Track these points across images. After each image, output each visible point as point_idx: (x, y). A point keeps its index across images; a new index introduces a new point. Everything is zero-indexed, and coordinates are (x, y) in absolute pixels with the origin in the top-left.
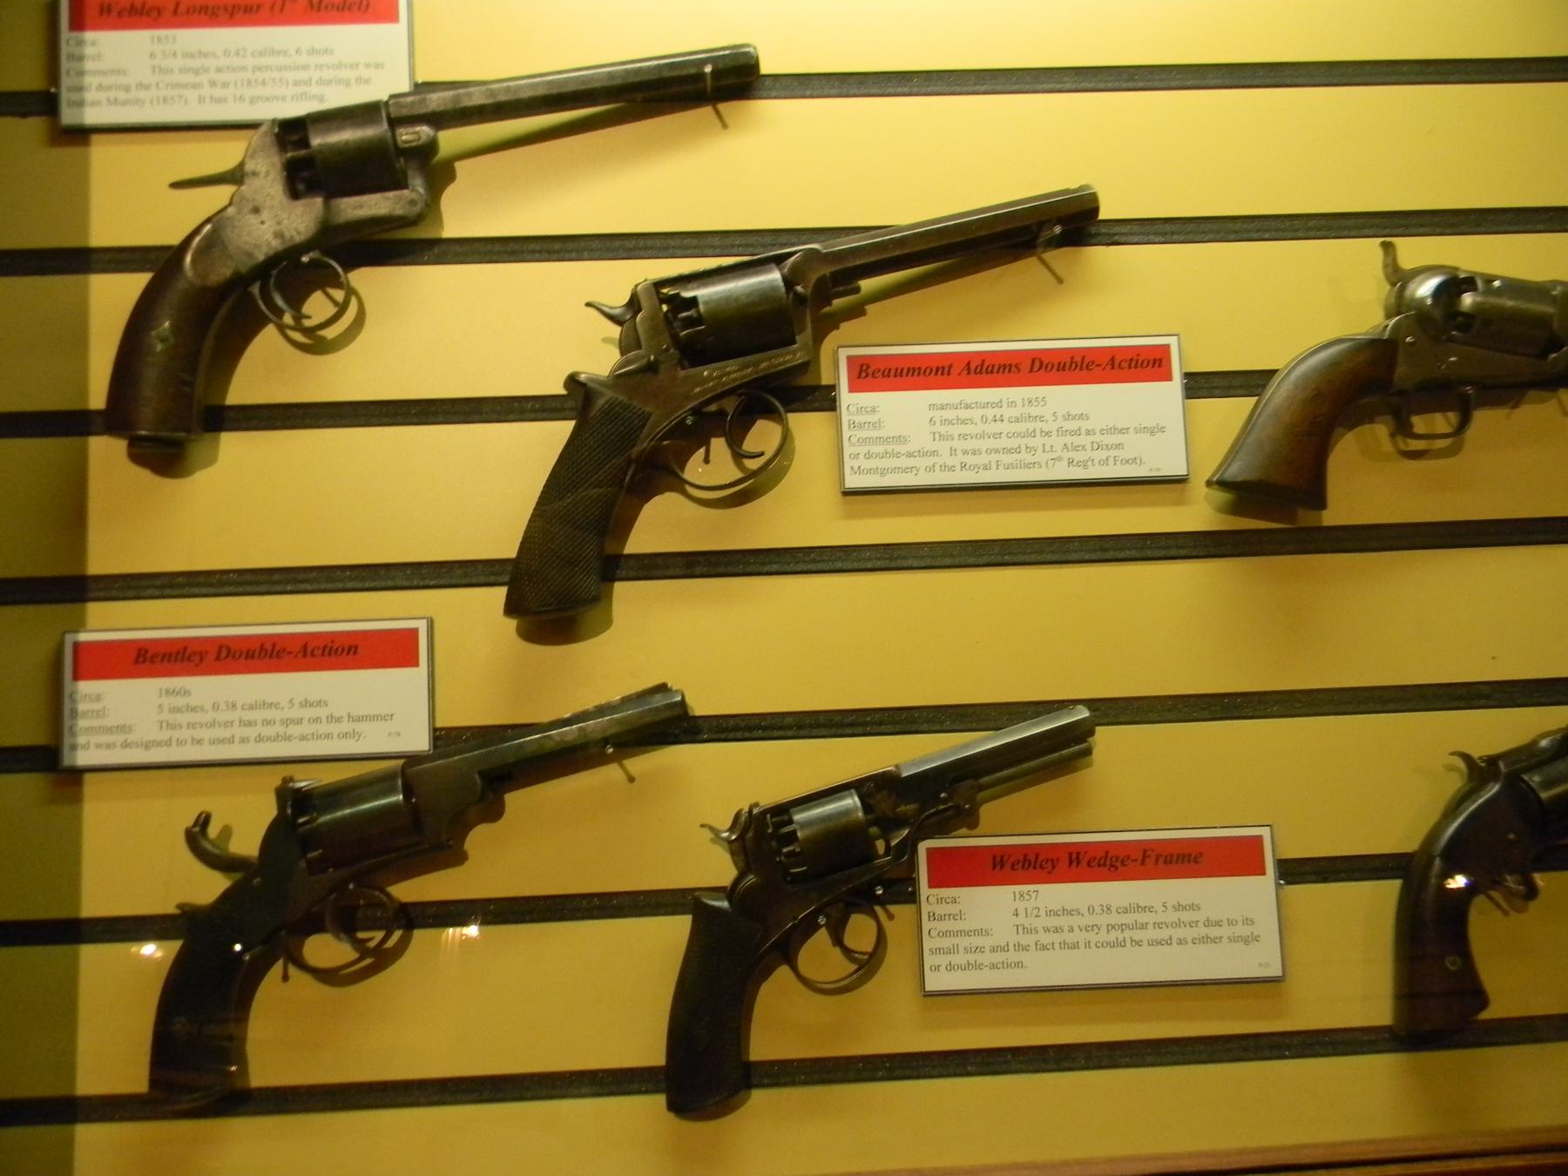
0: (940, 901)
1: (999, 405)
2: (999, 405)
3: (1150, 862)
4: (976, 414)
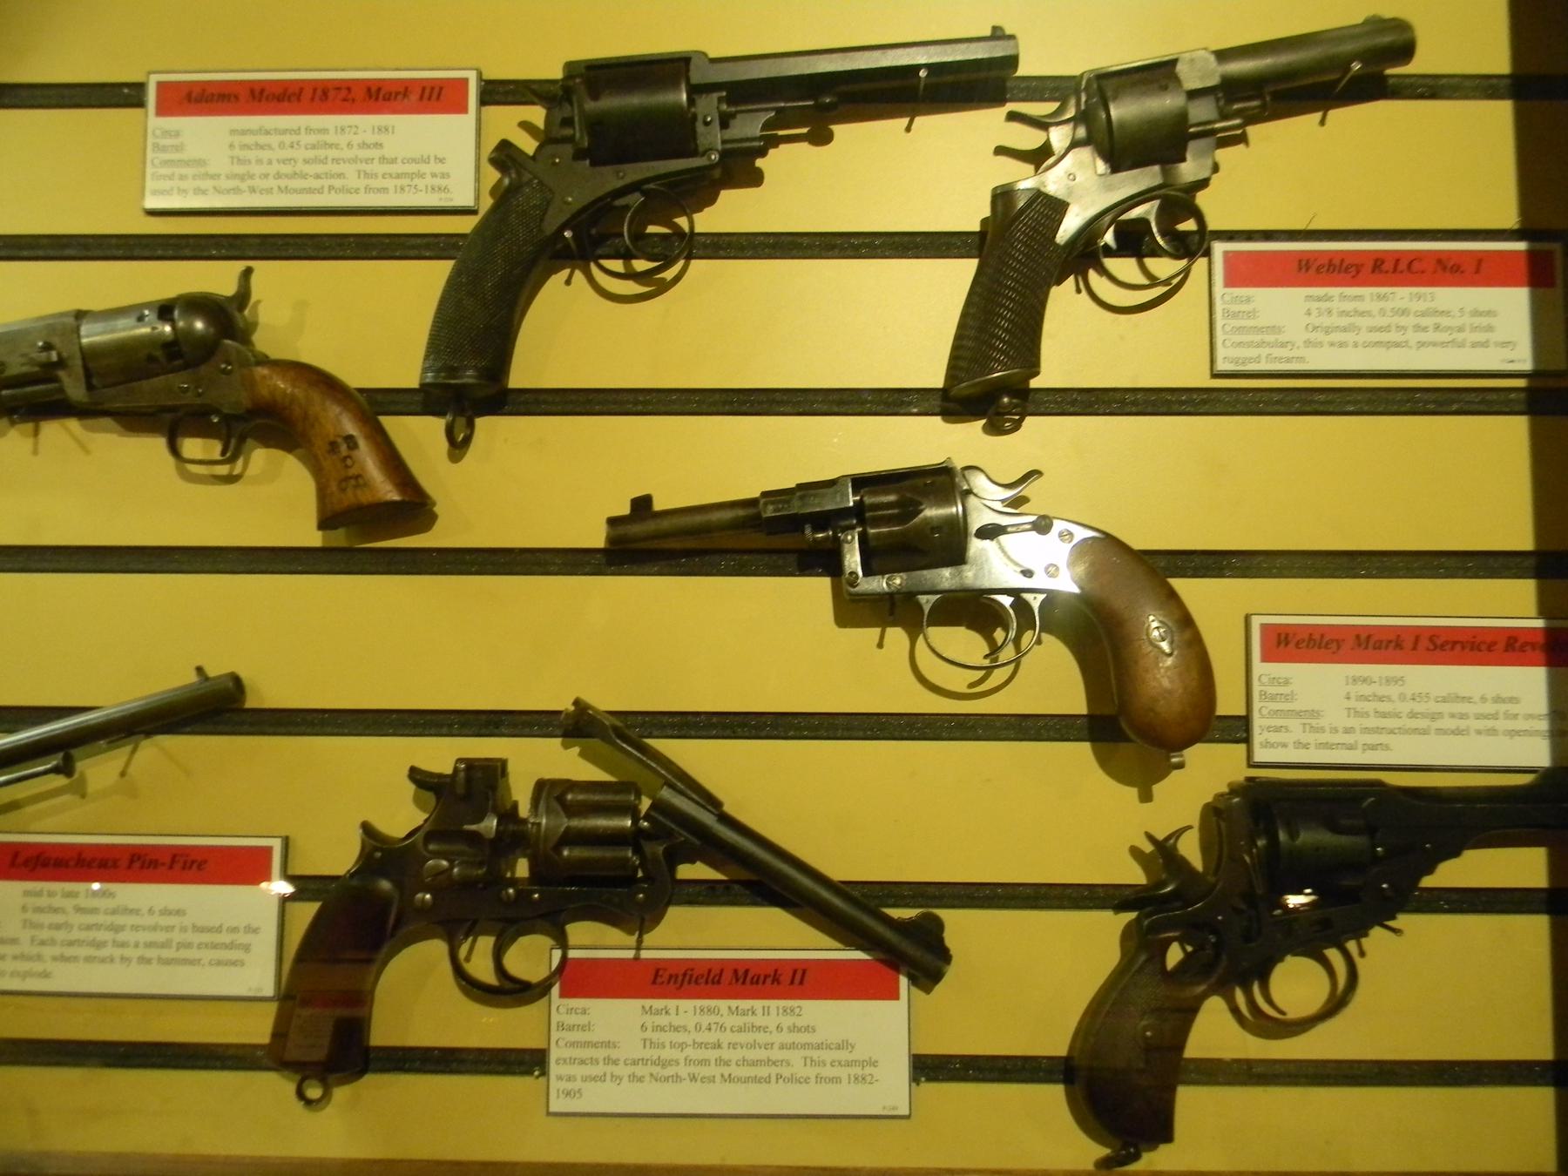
0: (570, 1011)
1: (297, 131)
2: (297, 131)
4: (274, 140)
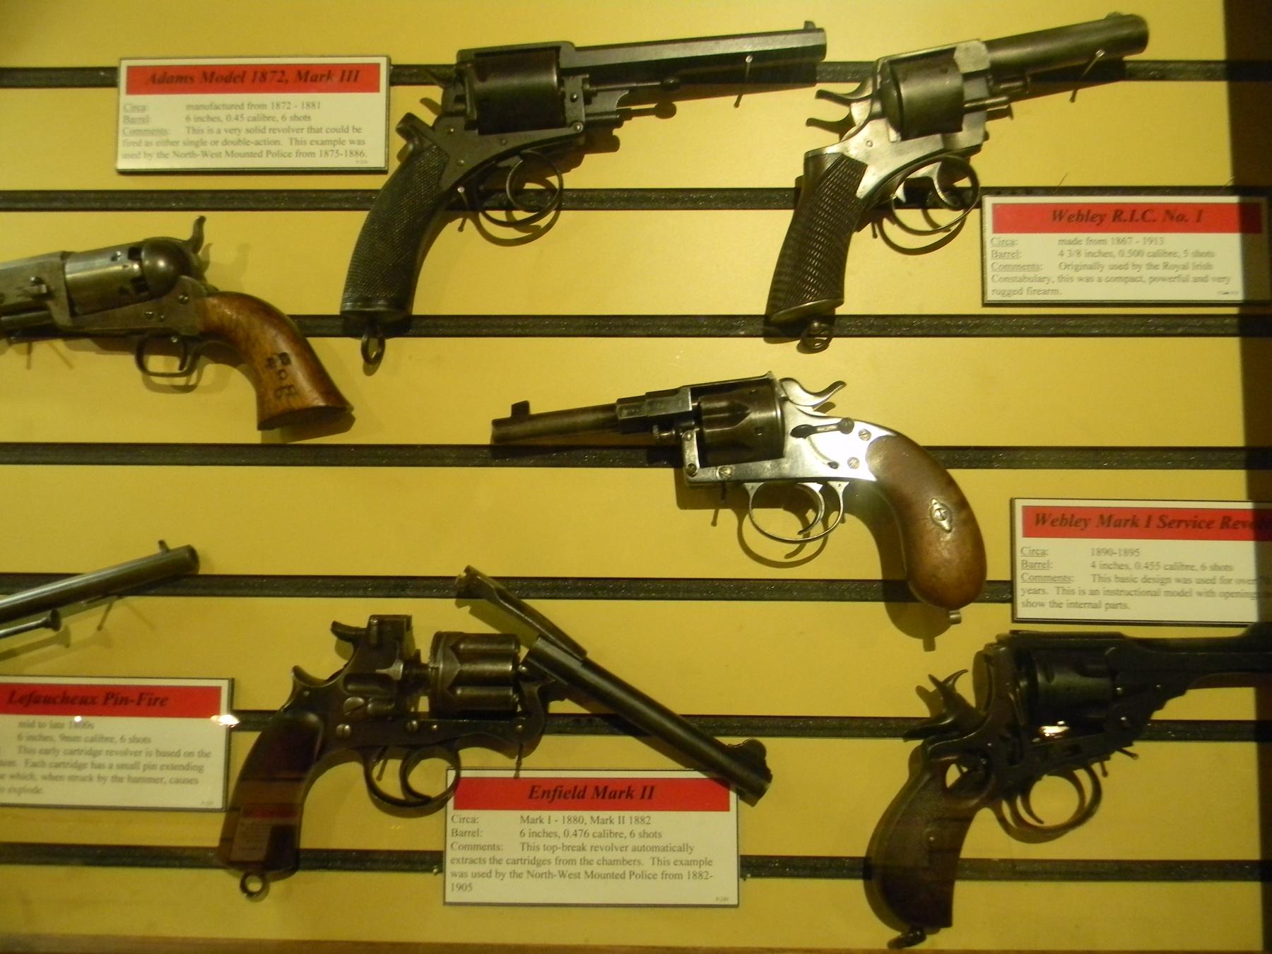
0: (463, 820)
1: (241, 107)
2: (241, 107)
3: (144, 703)
4: (222, 113)
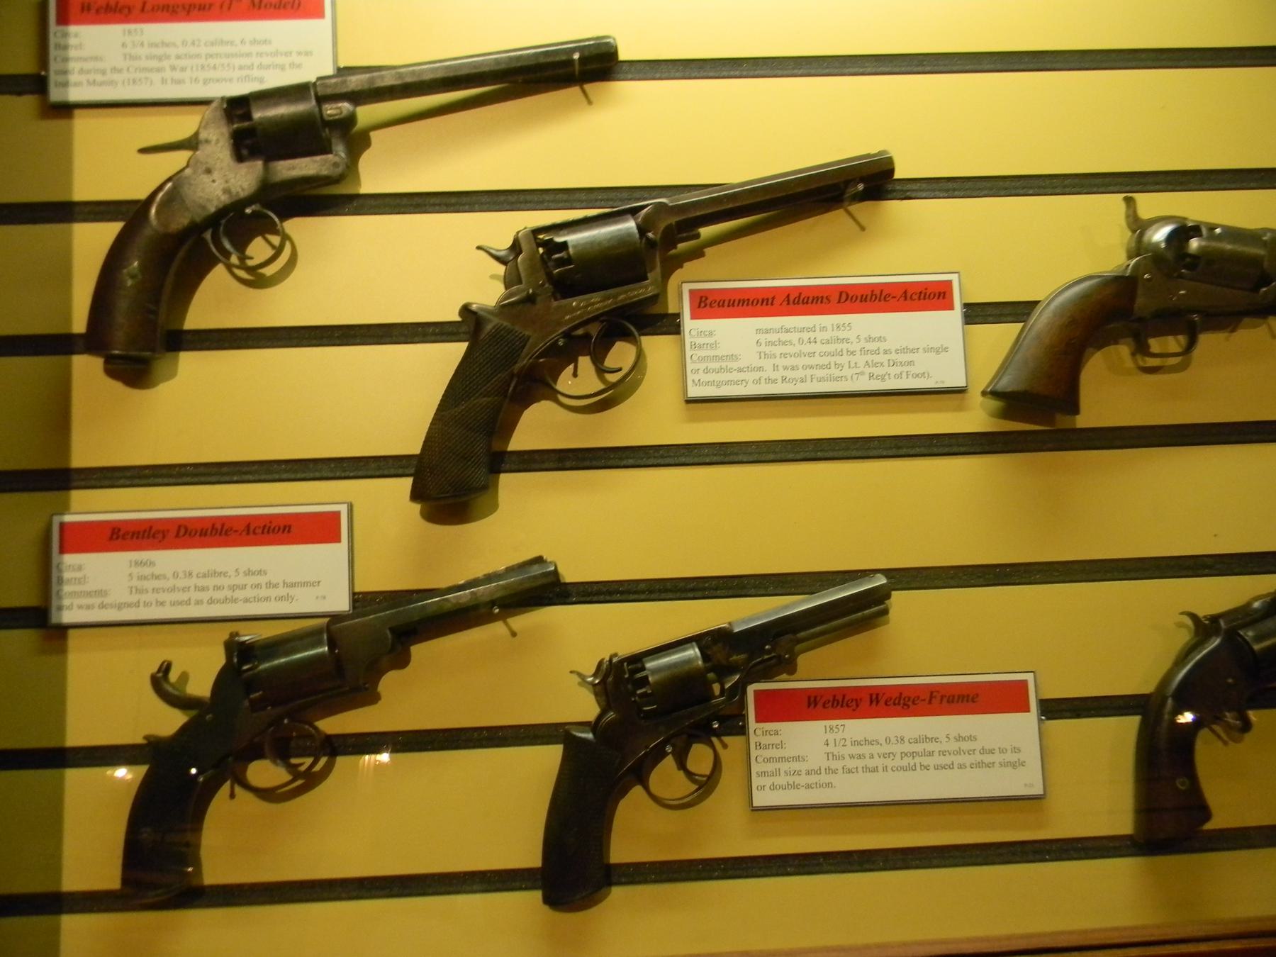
0: (765, 733)
1: (813, 329)
2: (813, 329)
4: (794, 337)
